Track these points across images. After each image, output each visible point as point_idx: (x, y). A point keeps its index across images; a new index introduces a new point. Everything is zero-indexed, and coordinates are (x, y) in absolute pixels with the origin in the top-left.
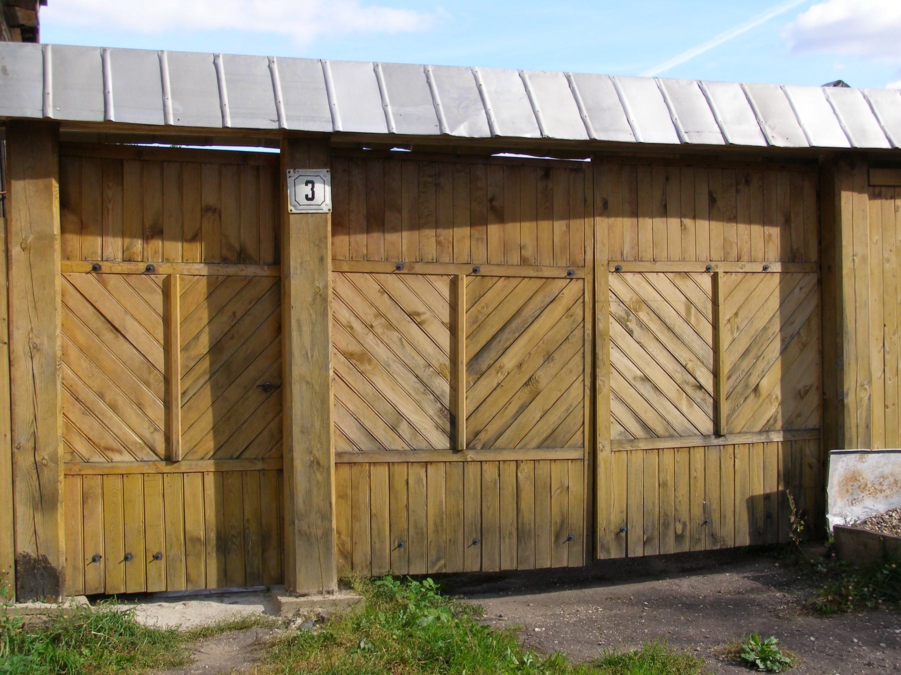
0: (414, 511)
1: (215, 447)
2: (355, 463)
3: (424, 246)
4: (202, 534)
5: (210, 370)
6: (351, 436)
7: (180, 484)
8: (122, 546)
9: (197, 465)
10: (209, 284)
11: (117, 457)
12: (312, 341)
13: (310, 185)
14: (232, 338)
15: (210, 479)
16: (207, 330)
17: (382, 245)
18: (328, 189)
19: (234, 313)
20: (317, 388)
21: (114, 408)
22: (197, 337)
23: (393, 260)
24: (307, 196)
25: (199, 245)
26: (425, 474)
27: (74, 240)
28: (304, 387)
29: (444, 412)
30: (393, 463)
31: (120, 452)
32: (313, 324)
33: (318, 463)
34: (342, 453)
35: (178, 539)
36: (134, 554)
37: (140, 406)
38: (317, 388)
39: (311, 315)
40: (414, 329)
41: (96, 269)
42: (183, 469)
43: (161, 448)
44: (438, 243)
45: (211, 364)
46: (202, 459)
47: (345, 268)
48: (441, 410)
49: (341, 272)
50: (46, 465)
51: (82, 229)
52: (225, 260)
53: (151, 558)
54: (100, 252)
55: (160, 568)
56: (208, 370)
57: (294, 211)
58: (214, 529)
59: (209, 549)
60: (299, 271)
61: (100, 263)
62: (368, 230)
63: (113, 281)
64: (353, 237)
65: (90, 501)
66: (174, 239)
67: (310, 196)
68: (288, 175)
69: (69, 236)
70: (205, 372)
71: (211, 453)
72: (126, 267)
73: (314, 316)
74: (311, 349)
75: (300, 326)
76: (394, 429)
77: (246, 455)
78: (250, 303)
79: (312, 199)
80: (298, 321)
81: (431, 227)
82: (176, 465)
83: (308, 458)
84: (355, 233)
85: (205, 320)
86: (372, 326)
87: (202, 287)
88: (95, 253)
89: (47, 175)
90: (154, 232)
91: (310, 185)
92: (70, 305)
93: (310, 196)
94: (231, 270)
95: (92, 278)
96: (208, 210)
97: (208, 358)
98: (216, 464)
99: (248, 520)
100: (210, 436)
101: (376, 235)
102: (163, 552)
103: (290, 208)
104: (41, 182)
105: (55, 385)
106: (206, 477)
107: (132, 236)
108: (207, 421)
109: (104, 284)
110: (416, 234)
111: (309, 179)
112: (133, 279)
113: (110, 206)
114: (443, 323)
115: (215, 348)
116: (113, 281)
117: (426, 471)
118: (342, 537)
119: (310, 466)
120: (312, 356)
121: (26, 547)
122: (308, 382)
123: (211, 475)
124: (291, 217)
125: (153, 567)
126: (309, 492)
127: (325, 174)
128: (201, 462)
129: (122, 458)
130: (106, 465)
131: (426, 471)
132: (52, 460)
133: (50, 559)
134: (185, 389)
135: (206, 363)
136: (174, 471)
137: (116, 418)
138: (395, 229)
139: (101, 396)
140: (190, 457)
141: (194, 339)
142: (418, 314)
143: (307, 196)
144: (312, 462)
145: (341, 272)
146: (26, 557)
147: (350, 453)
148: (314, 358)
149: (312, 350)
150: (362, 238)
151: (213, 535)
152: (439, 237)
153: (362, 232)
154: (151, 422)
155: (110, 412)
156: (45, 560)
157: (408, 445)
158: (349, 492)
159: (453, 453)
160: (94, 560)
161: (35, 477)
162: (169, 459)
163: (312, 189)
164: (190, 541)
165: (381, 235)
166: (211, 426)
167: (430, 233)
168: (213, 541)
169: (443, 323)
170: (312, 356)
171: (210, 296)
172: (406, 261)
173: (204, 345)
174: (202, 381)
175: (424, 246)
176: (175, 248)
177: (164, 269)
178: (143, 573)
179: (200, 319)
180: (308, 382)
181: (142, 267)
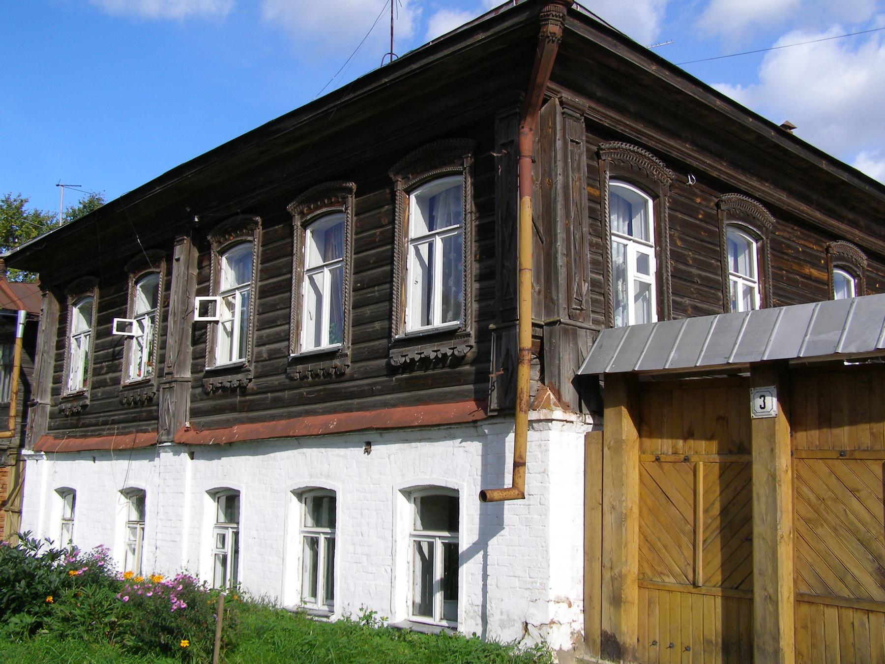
0: (859, 649)
1: (722, 579)
2: (813, 603)
3: (860, 437)
4: (714, 638)
5: (721, 527)
6: (810, 581)
7: (702, 602)
8: (668, 638)
9: (711, 590)
10: (720, 468)
11: (667, 579)
12: (766, 509)
13: (763, 398)
14: (734, 505)
15: (719, 600)
16: (719, 499)
17: (829, 438)
18: (775, 400)
19: (736, 488)
20: (769, 542)
21: (666, 547)
22: (713, 504)
23: (838, 449)
24: (761, 406)
25: (714, 442)
26: (867, 620)
27: (647, 442)
28: (761, 542)
29: (881, 571)
30: (841, 607)
31: (668, 576)
32: (767, 497)
33: (770, 597)
34: (803, 594)
35: (699, 639)
36: (674, 644)
37: (680, 547)
38: (769, 542)
39: (765, 490)
40: (855, 503)
41: (658, 459)
42: (703, 592)
43: (691, 577)
44: (872, 434)
45: (721, 522)
46: (714, 586)
47: (804, 456)
48: (879, 569)
49: (802, 459)
50: (616, 579)
51: (651, 436)
52: (731, 452)
53: (684, 649)
54: (660, 448)
55: (689, 657)
56: (719, 526)
57: (755, 417)
58: (721, 636)
59: (717, 649)
60: (758, 459)
61: (660, 456)
62: (820, 427)
63: (666, 466)
64: (809, 432)
65: (652, 605)
66: (700, 439)
67: (763, 406)
68: (751, 392)
69: (644, 439)
70: (717, 528)
71: (720, 583)
72: (676, 458)
73: (767, 491)
74: (766, 515)
75: (758, 498)
76: (842, 580)
77: (741, 587)
78: (746, 481)
79: (764, 408)
80: (758, 494)
81: (866, 422)
82: (699, 588)
83: (763, 593)
84: (810, 430)
85: (718, 493)
86: (823, 499)
87: (716, 470)
88: (658, 449)
89: (620, 405)
90: (689, 435)
91: (763, 398)
92: (644, 481)
93: (763, 406)
94: (733, 458)
95: (655, 464)
96: (720, 418)
97: (719, 518)
98: (723, 591)
99: (742, 634)
100: (719, 572)
101: (825, 430)
102: (691, 647)
103: (752, 415)
104: (617, 409)
105: (621, 530)
106: (717, 599)
107: (677, 438)
108: (717, 561)
109: (661, 467)
110: (854, 428)
111: (762, 394)
112: (677, 465)
113: (665, 420)
114: (878, 498)
115: (724, 512)
116: (666, 466)
117: (868, 617)
118: (805, 658)
119: (765, 599)
120: (766, 520)
121: (606, 627)
122: (764, 539)
123: (720, 598)
124: (753, 421)
125: (685, 654)
126: (764, 618)
127: (773, 389)
128: (713, 589)
129: (670, 580)
130: (660, 584)
131: (868, 617)
132: (619, 576)
133: (617, 636)
134: (705, 538)
135: (718, 522)
136: (697, 592)
137: (667, 554)
138: (839, 425)
139: (659, 539)
140: (707, 584)
141: (711, 505)
142: (858, 491)
143: (761, 406)
144: (767, 597)
145: (802, 459)
146: (606, 632)
147: (809, 595)
148: (768, 521)
149: (766, 515)
150: (815, 433)
151: (720, 640)
152: (872, 429)
153: (815, 429)
154: (685, 558)
155: (664, 550)
156: (614, 636)
157: (853, 594)
158: (809, 625)
159: (694, 588)
160: (686, 649)
161: (611, 585)
162: (695, 584)
163: (764, 401)
164: (707, 642)
165: (829, 430)
166: (720, 565)
167: (866, 426)
168: (720, 645)
169: (878, 498)
170: (766, 520)
171: (721, 476)
172: (848, 449)
173: (716, 510)
174: (715, 534)
175: (860, 437)
176: (698, 443)
177: (694, 459)
178: (680, 658)
179: (715, 492)
180: (764, 539)
181: (682, 457)
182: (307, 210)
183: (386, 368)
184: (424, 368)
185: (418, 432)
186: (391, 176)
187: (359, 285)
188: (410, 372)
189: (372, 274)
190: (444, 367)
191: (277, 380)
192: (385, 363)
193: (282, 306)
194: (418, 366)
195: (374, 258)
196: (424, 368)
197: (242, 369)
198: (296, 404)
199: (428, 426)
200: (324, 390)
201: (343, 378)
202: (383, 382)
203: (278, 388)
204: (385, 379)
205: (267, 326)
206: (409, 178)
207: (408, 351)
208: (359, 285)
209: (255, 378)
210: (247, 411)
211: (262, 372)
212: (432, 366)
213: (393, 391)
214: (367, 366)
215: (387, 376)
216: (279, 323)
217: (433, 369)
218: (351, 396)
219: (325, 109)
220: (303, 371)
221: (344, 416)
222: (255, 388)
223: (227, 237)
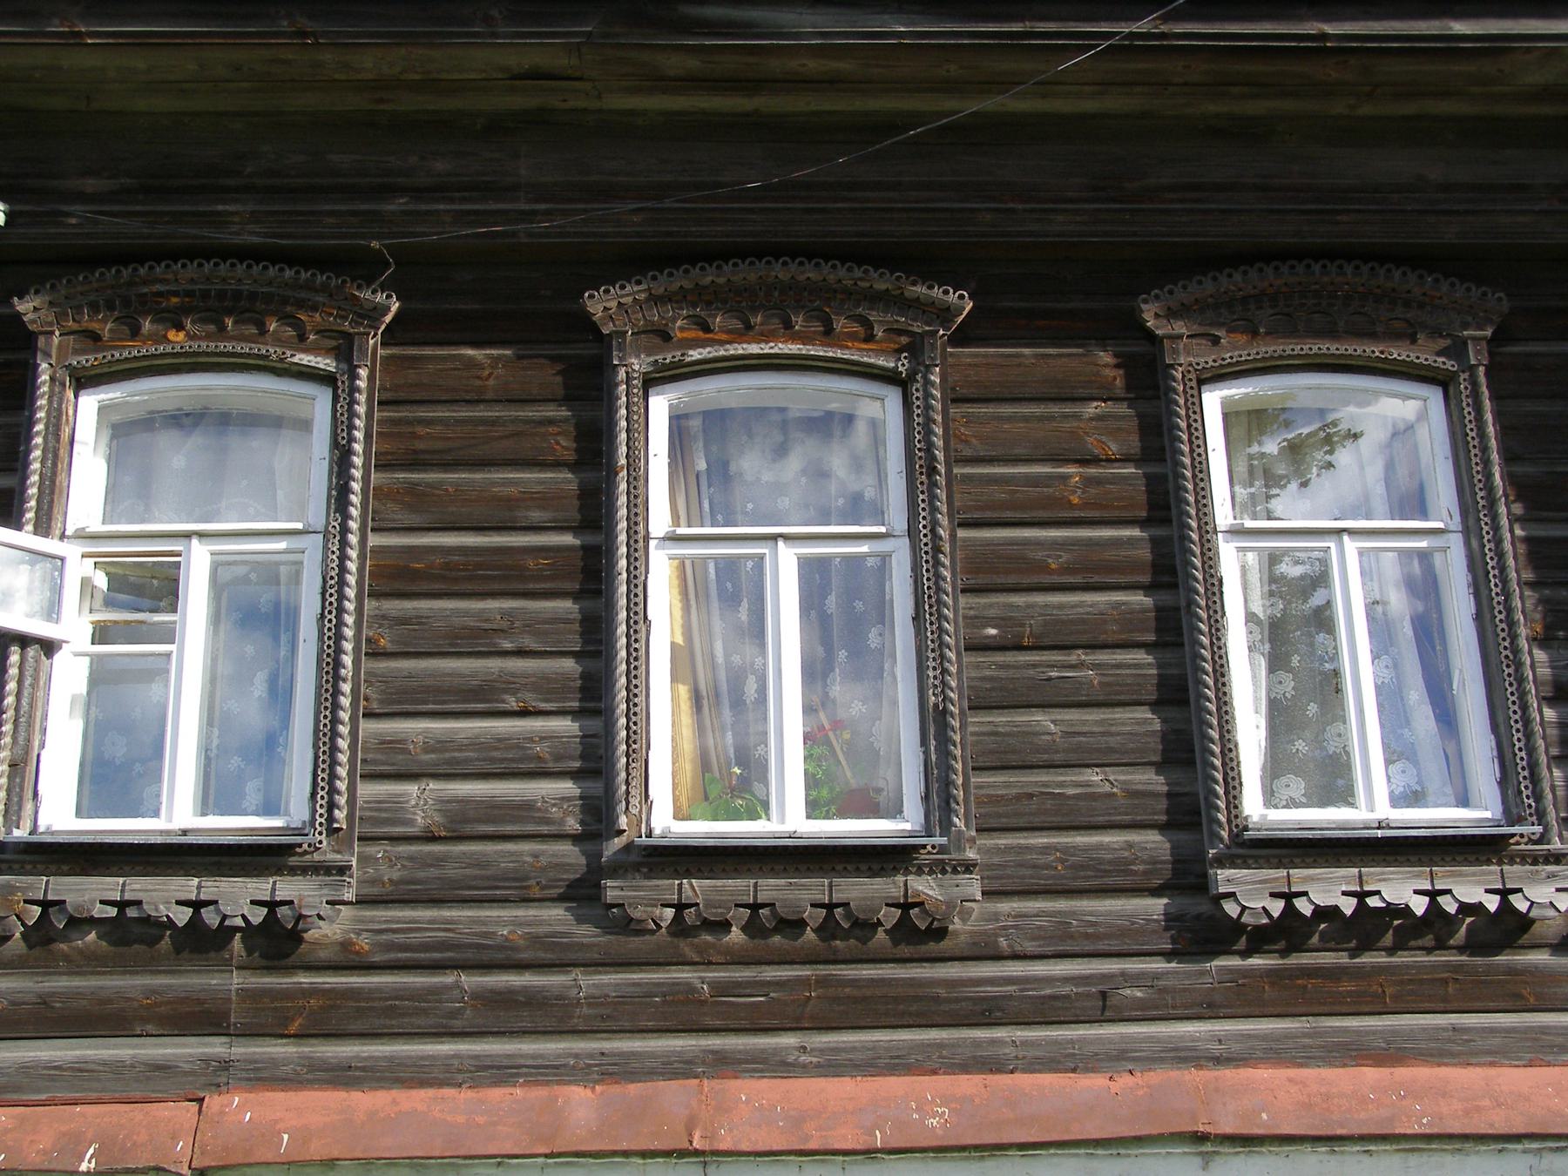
182: (111, 330)
183: (1167, 929)
184: (1353, 944)
185: (1397, 1158)
186: (1145, 316)
187: (993, 632)
188: (1284, 953)
189: (1061, 606)
190: (1441, 946)
191: (517, 923)
192: (1161, 910)
193: (530, 643)
194: (1322, 934)
195: (1065, 557)
196: (1353, 944)
197: (293, 861)
198: (745, 1024)
199: (1450, 1137)
200: (823, 982)
201: (932, 947)
202: (1157, 976)
203: (525, 956)
204: (1158, 965)
205: (431, 707)
206: (222, 328)
207: (1306, 880)
208: (993, 632)
209: (362, 901)
210: (299, 1036)
211: (401, 882)
212: (1388, 939)
213: (1208, 1009)
214: (1072, 914)
215: (1169, 955)
216: (512, 703)
217: (1391, 951)
218: (988, 1012)
219: (1016, 27)
220: (709, 904)
221: (968, 1084)
222: (364, 942)
223: (147, 326)
